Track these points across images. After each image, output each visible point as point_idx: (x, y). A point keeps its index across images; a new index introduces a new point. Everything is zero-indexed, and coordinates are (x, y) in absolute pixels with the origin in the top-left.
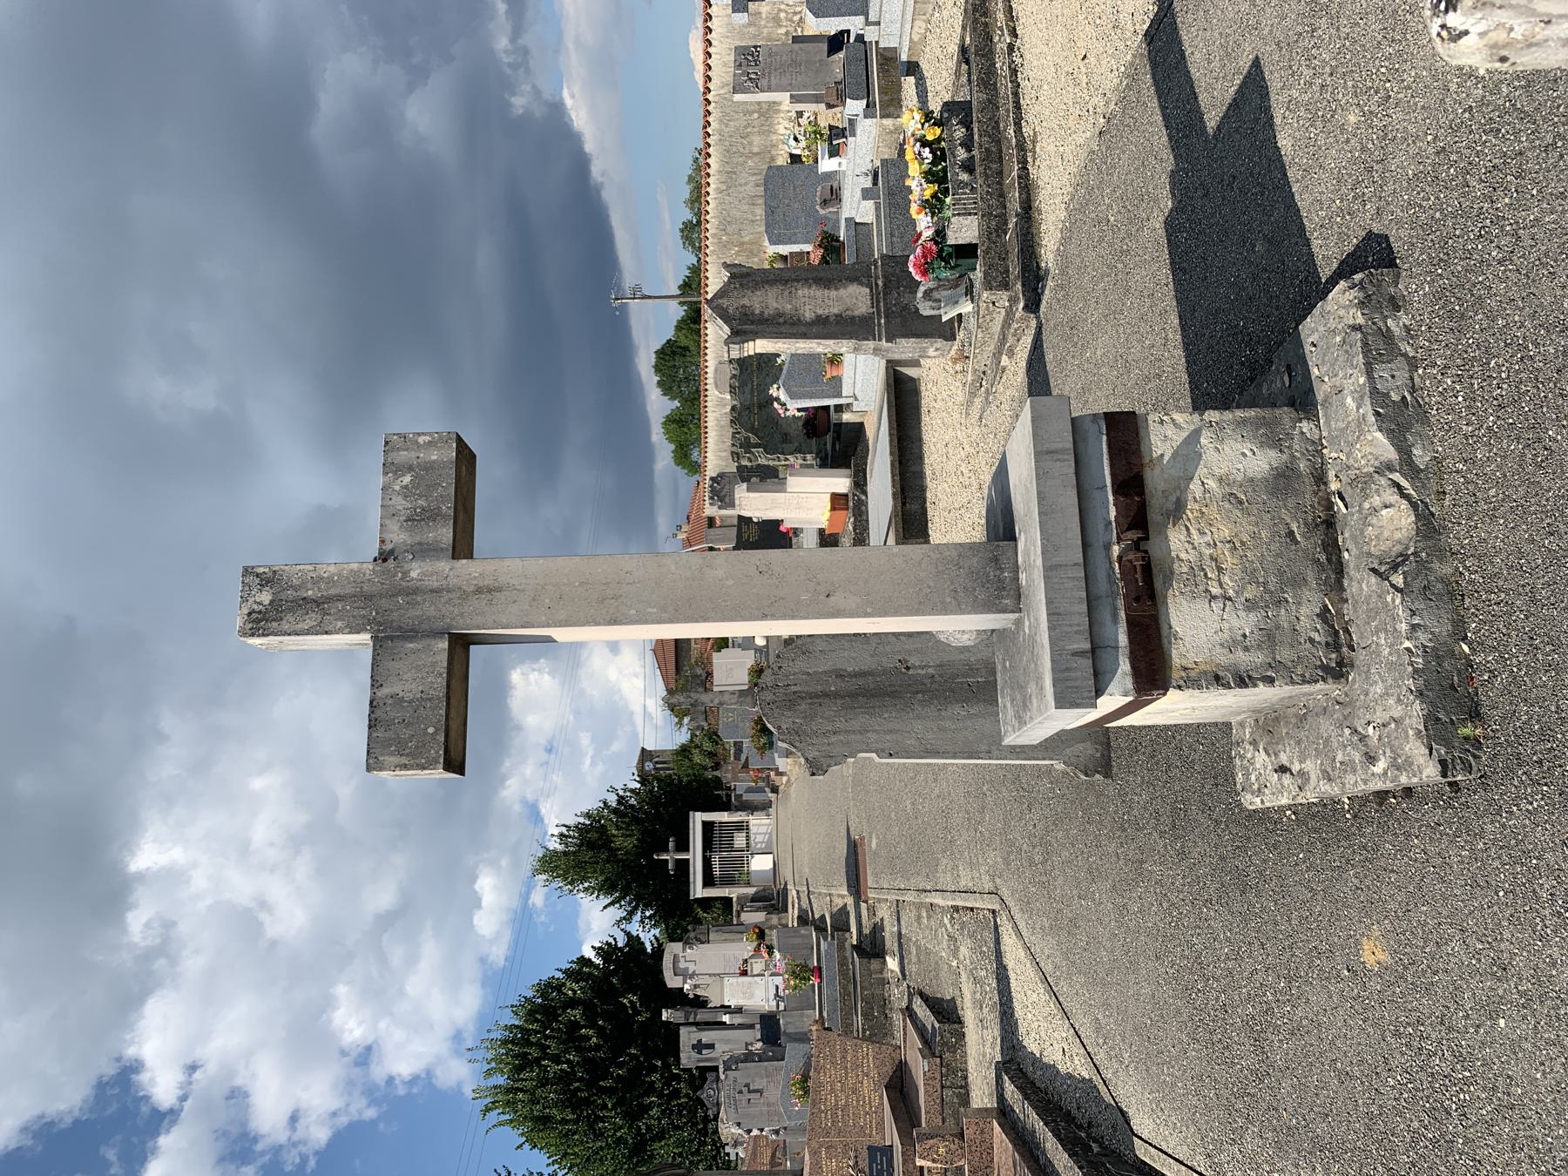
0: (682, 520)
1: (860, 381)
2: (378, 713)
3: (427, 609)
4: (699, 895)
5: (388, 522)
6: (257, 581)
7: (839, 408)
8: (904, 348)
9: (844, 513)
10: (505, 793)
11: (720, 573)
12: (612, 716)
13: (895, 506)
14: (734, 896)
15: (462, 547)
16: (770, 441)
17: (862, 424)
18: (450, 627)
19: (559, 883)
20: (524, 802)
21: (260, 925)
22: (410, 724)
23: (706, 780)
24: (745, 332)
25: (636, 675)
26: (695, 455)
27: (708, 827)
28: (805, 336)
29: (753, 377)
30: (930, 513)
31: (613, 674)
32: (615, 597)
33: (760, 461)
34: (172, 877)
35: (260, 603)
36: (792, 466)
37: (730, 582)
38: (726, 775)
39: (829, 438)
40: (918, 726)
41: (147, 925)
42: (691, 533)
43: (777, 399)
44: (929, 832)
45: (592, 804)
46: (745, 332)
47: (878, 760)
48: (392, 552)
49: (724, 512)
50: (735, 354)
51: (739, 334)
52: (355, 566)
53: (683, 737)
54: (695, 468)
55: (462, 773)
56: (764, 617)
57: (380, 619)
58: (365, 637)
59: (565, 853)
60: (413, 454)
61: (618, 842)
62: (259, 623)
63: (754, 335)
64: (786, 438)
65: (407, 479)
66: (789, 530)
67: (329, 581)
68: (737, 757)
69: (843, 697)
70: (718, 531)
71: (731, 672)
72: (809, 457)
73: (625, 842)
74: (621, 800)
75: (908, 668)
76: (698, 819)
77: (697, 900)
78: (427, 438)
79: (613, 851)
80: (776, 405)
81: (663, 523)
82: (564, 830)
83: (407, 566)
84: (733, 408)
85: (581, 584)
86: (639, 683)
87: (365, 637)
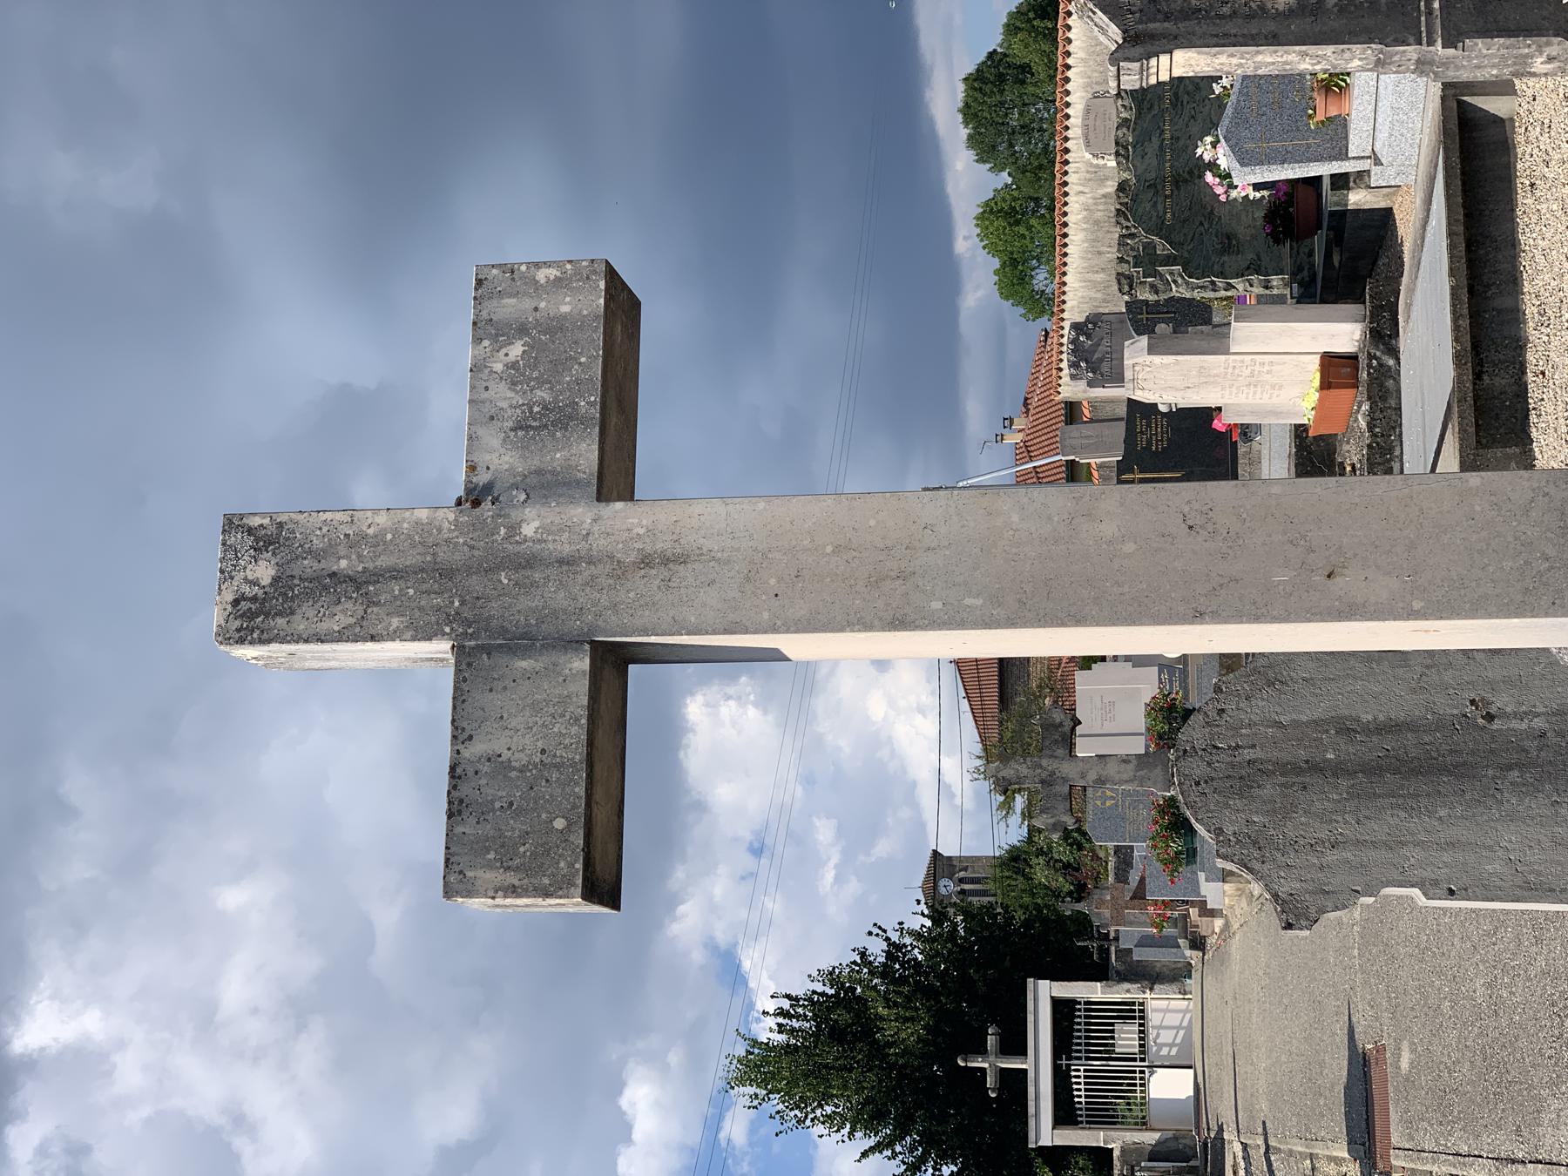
0: (1013, 407)
1: (1388, 123)
2: (465, 790)
3: (551, 596)
4: (1046, 1141)
5: (481, 432)
6: (250, 541)
7: (1341, 182)
8: (1481, 58)
9: (1349, 392)
10: (675, 929)
11: (1109, 529)
12: (874, 791)
13: (1459, 381)
14: (1116, 1147)
15: (615, 479)
16: (1192, 251)
17: (1388, 212)
18: (594, 629)
19: (775, 1103)
20: (711, 946)
21: (235, 1158)
22: (520, 812)
23: (1060, 917)
24: (1152, 37)
25: (921, 710)
26: (1040, 278)
27: (1063, 1010)
28: (1274, 40)
29: (1162, 126)
30: (1534, 394)
31: (877, 708)
32: (902, 576)
33: (1175, 292)
34: (82, 1064)
35: (255, 583)
36: (1241, 300)
37: (1129, 547)
38: (1099, 910)
39: (1318, 242)
40: (1509, 836)
41: (42, 1151)
42: (1032, 432)
43: (1213, 166)
44: (1523, 1043)
45: (838, 955)
46: (1152, 37)
47: (1422, 901)
48: (488, 488)
49: (1099, 392)
50: (1131, 82)
51: (1140, 42)
52: (423, 514)
53: (1013, 833)
54: (1043, 304)
55: (615, 904)
56: (1198, 616)
57: (467, 614)
58: (441, 647)
59: (788, 1049)
60: (528, 304)
61: (889, 1030)
62: (254, 618)
63: (1170, 43)
64: (1229, 243)
65: (516, 350)
66: (1231, 428)
67: (378, 541)
68: (1122, 877)
69: (1352, 774)
70: (1086, 430)
71: (1112, 720)
72: (1276, 280)
73: (902, 1031)
74: (894, 950)
75: (1490, 717)
76: (1043, 993)
77: (1042, 1150)
78: (553, 273)
79: (878, 1050)
80: (1209, 177)
81: (976, 414)
82: (786, 1004)
83: (515, 515)
84: (1122, 187)
85: (837, 550)
86: (929, 726)
87: (441, 647)
